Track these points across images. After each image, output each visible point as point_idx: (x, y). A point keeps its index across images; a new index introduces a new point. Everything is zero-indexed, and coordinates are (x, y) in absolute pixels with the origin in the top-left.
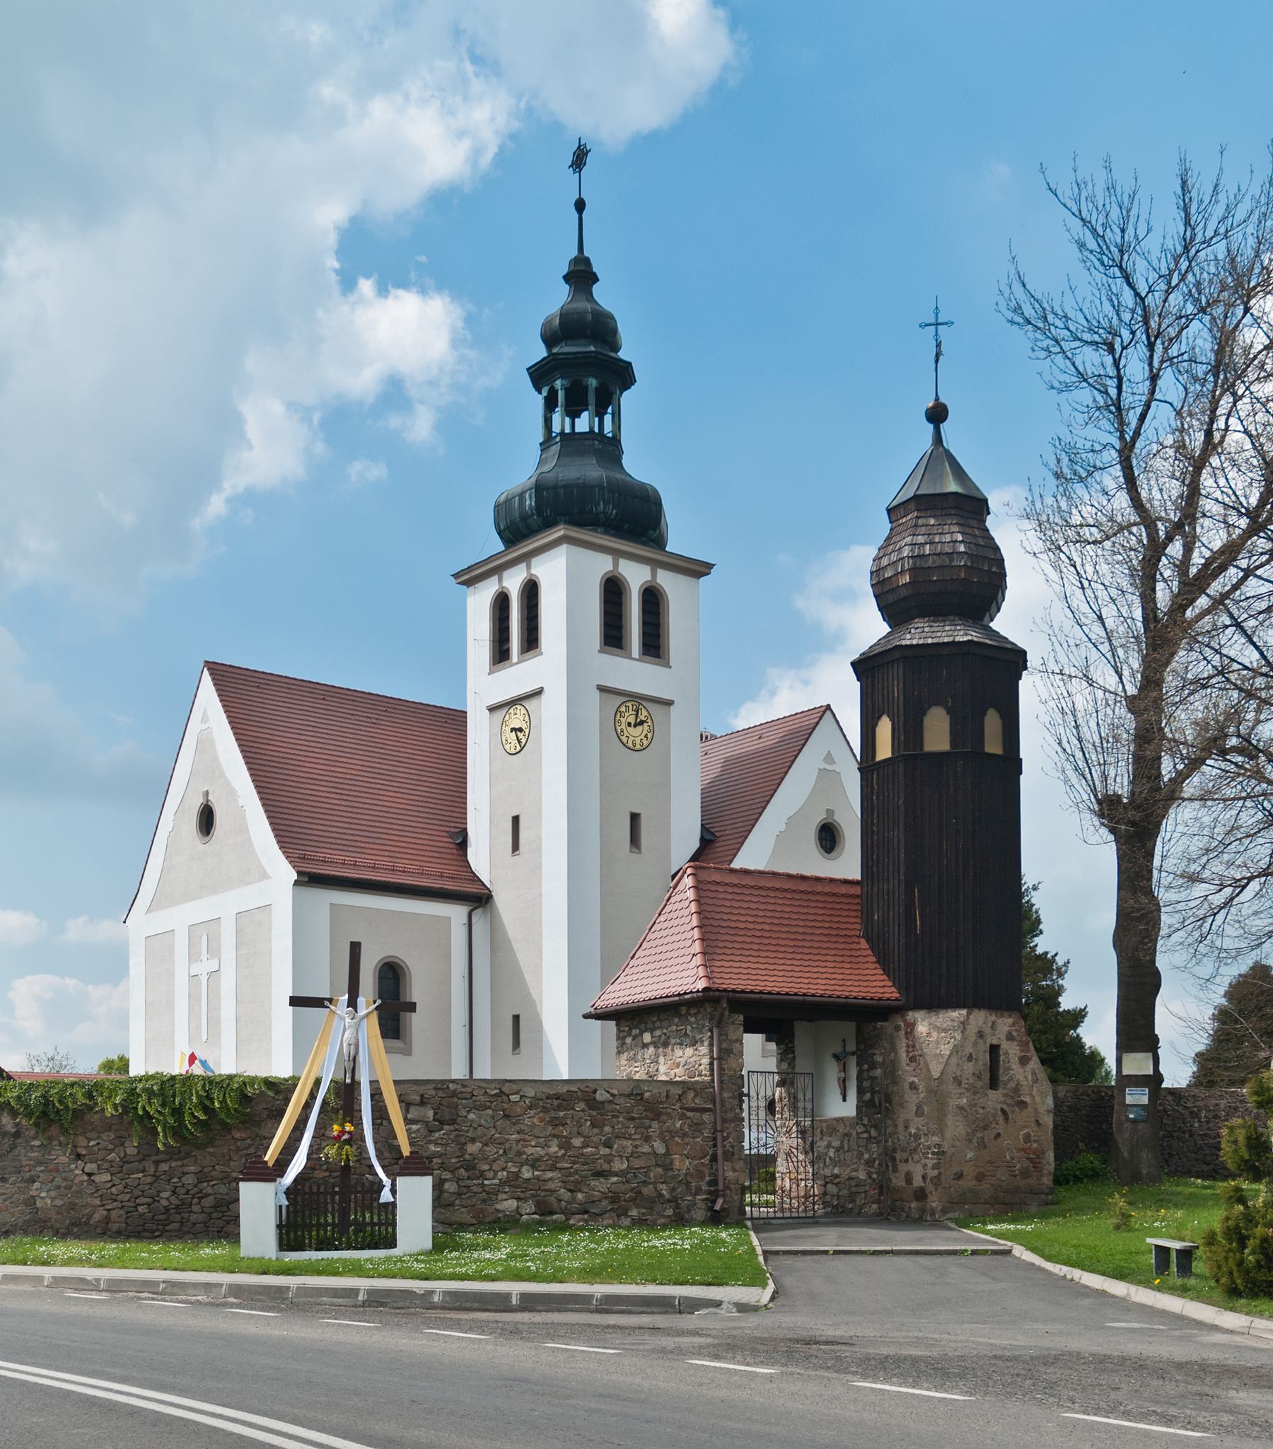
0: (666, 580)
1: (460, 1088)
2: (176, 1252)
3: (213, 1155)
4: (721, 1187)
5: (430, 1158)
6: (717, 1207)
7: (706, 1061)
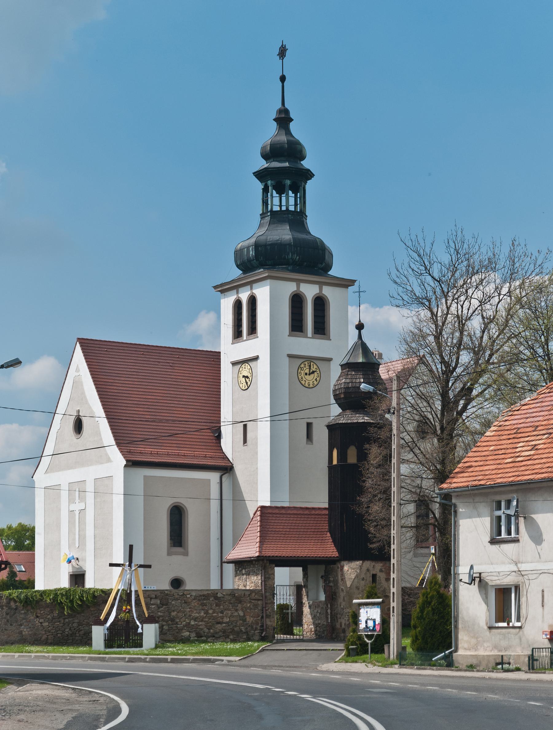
0: (328, 292)
1: (169, 593)
2: (71, 649)
3: (84, 616)
4: (265, 628)
5: (158, 618)
6: (263, 635)
7: (260, 582)
